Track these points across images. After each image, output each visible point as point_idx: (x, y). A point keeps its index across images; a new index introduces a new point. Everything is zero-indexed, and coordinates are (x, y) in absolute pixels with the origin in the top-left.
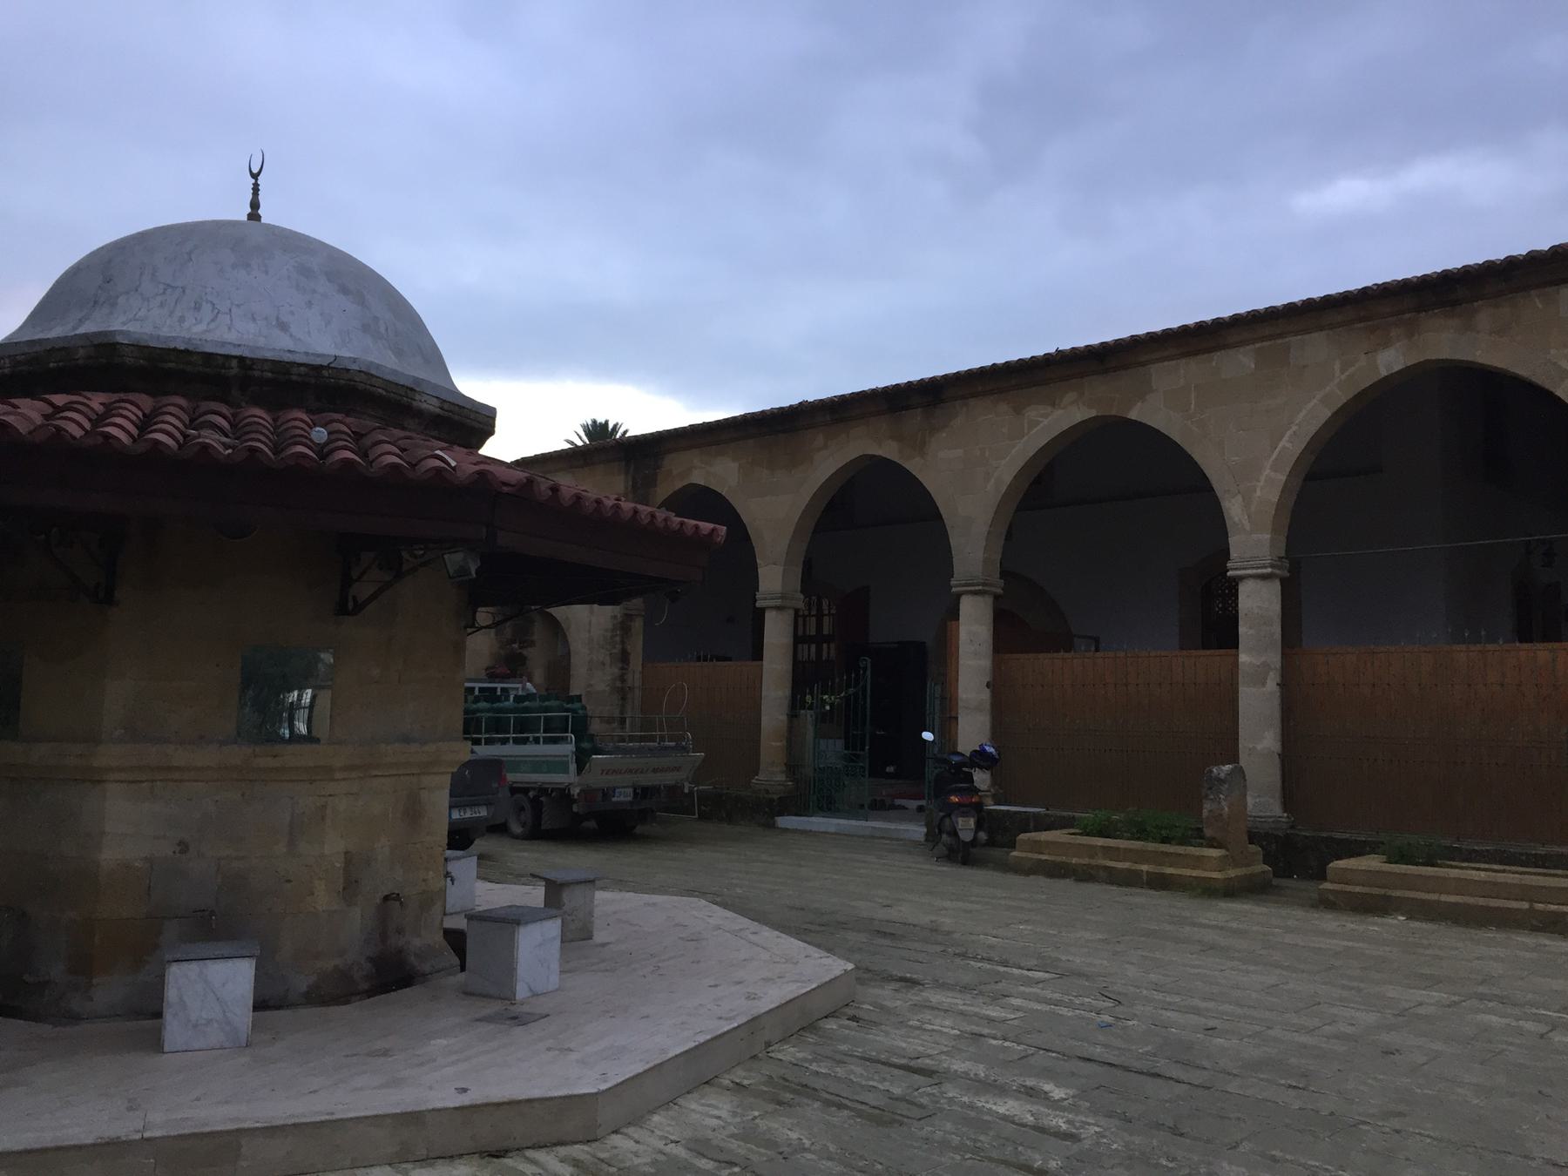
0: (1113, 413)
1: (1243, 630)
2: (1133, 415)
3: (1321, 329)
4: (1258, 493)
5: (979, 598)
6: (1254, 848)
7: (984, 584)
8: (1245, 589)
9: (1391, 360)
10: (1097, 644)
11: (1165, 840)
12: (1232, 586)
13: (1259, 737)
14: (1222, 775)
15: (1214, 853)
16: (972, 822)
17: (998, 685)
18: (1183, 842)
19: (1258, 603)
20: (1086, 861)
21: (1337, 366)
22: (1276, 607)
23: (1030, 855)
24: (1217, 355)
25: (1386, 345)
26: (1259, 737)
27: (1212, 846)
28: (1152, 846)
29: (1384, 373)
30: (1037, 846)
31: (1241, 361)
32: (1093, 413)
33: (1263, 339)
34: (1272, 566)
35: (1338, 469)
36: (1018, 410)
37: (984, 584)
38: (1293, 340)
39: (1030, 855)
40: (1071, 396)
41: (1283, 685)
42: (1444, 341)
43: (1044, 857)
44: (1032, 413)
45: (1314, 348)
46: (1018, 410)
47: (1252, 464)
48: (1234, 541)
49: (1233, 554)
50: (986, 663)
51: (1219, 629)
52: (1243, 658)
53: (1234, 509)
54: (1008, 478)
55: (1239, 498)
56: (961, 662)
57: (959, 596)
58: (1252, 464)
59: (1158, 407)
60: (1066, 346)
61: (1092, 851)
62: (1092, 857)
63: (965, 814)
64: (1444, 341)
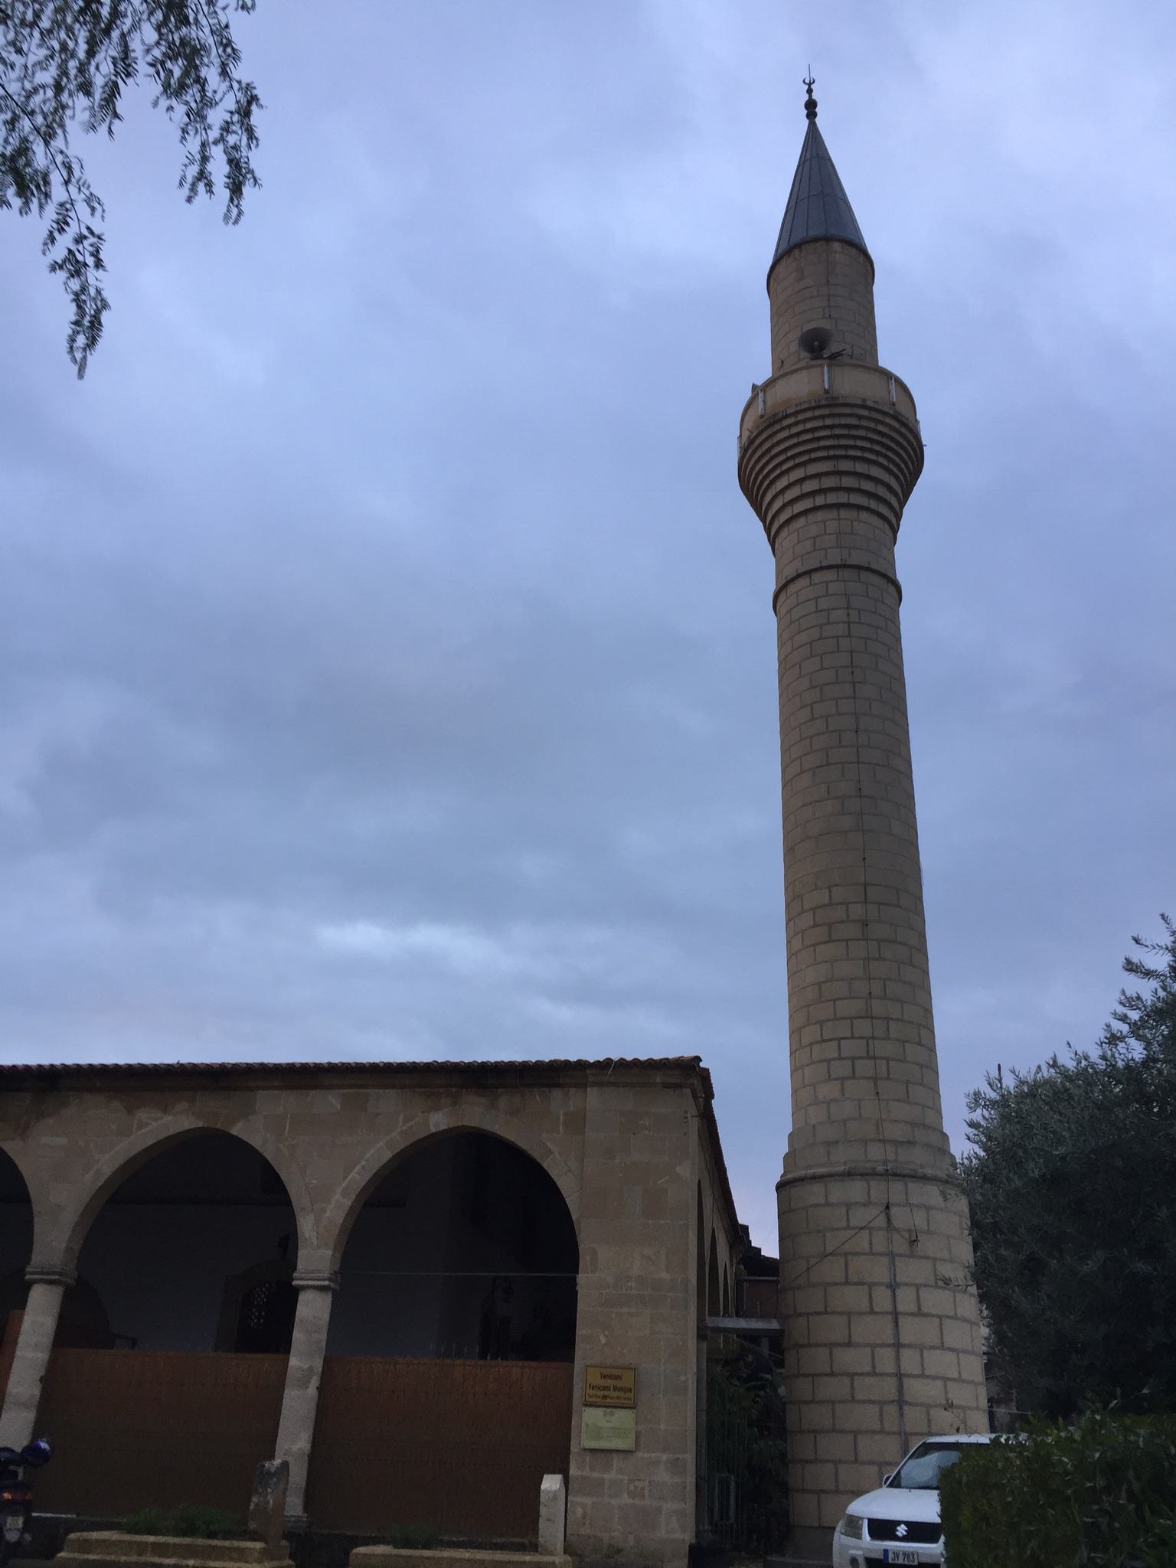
0: (219, 1126)
1: (297, 1335)
2: (236, 1130)
3: (393, 1087)
4: (328, 1214)
5: (323, 1294)
6: (284, 1543)
7: (60, 1274)
8: (304, 1298)
9: (439, 1121)
10: (134, 1343)
11: (212, 1535)
12: (295, 1292)
13: (294, 1440)
14: (273, 1470)
15: (258, 1545)
16: (20, 1521)
17: (50, 1379)
18: (227, 1535)
19: (313, 1311)
20: (134, 1558)
21: (401, 1118)
22: (325, 1316)
23: (76, 1555)
24: (312, 1093)
25: (437, 1109)
26: (294, 1440)
27: (254, 1540)
28: (200, 1541)
29: (433, 1130)
30: (85, 1546)
31: (330, 1101)
32: (200, 1124)
33: (351, 1086)
34: (330, 1280)
35: (383, 1201)
36: (130, 1111)
37: (60, 1274)
38: (372, 1092)
39: (76, 1555)
40: (185, 1105)
41: (320, 1389)
42: (474, 1113)
43: (91, 1557)
44: (142, 1115)
45: (386, 1101)
46: (130, 1111)
47: (325, 1184)
48: (302, 1253)
49: (300, 1266)
50: (43, 1356)
51: (274, 1335)
52: (293, 1362)
53: (306, 1226)
54: (107, 1171)
55: (312, 1215)
56: (18, 1353)
57: (29, 1285)
58: (325, 1184)
59: (258, 1128)
60: (184, 1060)
61: (142, 1548)
62: (140, 1554)
63: (15, 1513)
64: (474, 1113)
